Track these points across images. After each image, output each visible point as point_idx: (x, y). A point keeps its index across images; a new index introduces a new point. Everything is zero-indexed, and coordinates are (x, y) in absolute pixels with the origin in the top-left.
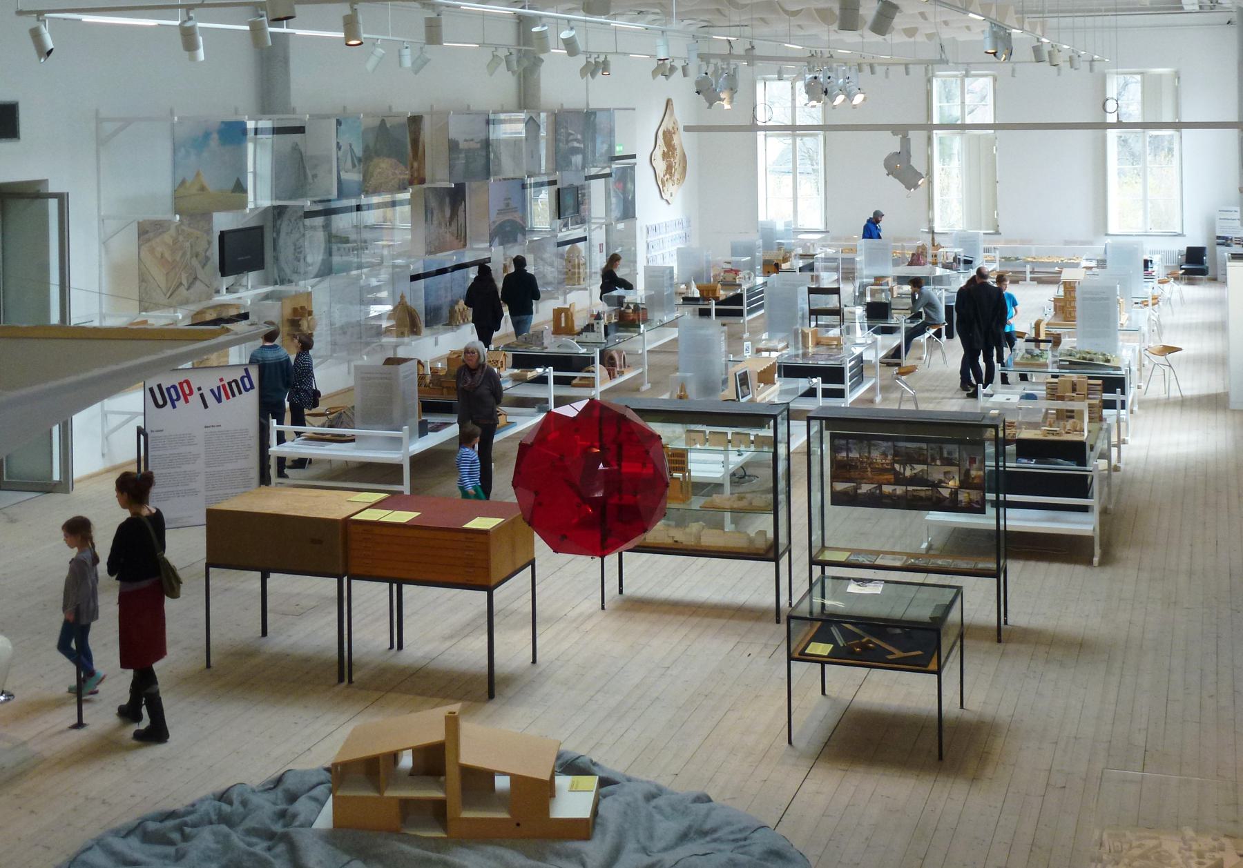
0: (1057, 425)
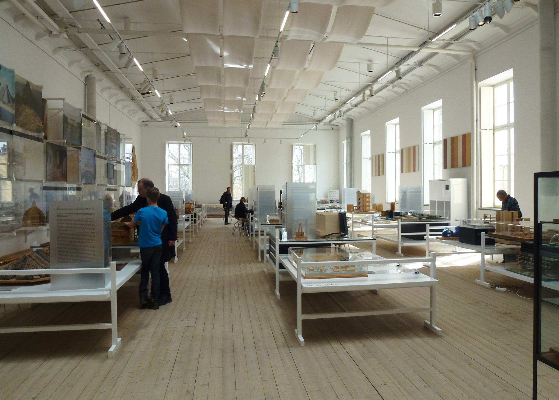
0: (504, 226)
